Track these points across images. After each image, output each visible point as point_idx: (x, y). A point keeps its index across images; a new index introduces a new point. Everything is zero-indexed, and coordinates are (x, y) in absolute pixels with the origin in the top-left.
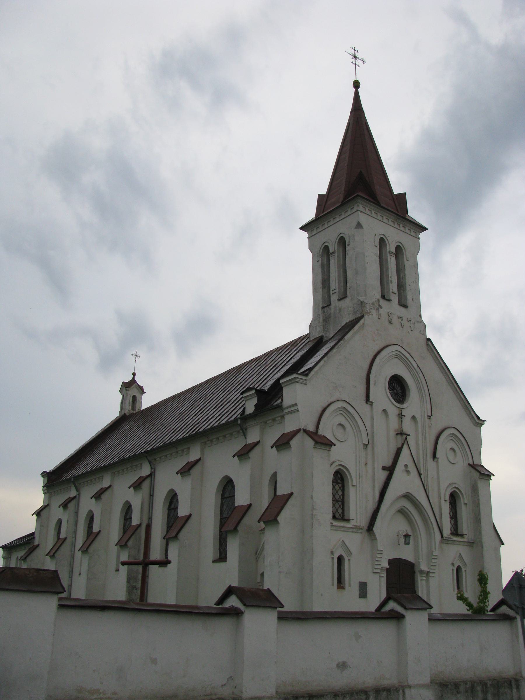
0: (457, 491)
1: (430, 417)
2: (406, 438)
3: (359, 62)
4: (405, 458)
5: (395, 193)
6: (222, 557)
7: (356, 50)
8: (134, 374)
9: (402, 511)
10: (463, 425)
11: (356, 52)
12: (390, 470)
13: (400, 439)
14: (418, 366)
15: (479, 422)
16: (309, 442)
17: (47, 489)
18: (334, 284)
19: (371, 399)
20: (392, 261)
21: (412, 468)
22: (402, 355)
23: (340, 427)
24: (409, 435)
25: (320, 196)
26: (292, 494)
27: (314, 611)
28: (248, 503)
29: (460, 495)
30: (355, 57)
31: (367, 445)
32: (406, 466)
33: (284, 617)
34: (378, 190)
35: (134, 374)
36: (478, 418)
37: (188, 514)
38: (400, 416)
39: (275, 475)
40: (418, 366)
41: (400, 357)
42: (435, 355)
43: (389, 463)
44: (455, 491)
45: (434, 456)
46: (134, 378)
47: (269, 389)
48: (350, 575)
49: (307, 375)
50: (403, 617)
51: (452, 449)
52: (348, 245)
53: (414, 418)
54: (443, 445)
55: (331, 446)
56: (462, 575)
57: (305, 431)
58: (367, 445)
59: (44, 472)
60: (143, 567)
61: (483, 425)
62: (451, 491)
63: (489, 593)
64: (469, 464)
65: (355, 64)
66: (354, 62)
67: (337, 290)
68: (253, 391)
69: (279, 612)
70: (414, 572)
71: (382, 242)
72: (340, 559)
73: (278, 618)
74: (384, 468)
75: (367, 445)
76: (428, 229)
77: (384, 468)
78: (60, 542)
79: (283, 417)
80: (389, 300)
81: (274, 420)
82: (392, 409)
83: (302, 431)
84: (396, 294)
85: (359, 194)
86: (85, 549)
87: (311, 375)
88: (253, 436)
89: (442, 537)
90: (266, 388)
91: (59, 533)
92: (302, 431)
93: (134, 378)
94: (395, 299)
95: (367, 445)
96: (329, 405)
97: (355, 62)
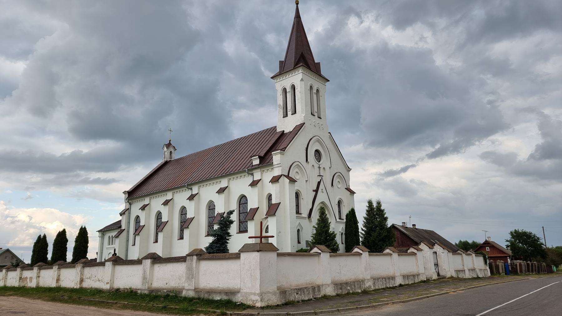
0: (298, 191)
5: (316, 62)
8: (170, 141)
12: (316, 191)
15: (349, 170)
16: (287, 181)
17: (511, 237)
20: (315, 96)
21: (324, 190)
23: (297, 173)
25: (281, 62)
32: (322, 189)
33: (280, 255)
34: (309, 62)
35: (170, 141)
36: (349, 168)
37: (224, 212)
38: (319, 167)
41: (318, 141)
43: (315, 188)
44: (340, 200)
45: (332, 185)
46: (170, 142)
48: (302, 237)
54: (336, 180)
55: (295, 182)
56: (300, 233)
57: (284, 175)
58: (307, 181)
63: (460, 241)
64: (345, 188)
67: (291, 110)
68: (258, 157)
71: (311, 87)
72: (298, 231)
73: (277, 255)
74: (314, 191)
77: (314, 191)
80: (314, 115)
81: (268, 170)
89: (336, 220)
93: (170, 142)
95: (307, 181)
96: (311, 139)
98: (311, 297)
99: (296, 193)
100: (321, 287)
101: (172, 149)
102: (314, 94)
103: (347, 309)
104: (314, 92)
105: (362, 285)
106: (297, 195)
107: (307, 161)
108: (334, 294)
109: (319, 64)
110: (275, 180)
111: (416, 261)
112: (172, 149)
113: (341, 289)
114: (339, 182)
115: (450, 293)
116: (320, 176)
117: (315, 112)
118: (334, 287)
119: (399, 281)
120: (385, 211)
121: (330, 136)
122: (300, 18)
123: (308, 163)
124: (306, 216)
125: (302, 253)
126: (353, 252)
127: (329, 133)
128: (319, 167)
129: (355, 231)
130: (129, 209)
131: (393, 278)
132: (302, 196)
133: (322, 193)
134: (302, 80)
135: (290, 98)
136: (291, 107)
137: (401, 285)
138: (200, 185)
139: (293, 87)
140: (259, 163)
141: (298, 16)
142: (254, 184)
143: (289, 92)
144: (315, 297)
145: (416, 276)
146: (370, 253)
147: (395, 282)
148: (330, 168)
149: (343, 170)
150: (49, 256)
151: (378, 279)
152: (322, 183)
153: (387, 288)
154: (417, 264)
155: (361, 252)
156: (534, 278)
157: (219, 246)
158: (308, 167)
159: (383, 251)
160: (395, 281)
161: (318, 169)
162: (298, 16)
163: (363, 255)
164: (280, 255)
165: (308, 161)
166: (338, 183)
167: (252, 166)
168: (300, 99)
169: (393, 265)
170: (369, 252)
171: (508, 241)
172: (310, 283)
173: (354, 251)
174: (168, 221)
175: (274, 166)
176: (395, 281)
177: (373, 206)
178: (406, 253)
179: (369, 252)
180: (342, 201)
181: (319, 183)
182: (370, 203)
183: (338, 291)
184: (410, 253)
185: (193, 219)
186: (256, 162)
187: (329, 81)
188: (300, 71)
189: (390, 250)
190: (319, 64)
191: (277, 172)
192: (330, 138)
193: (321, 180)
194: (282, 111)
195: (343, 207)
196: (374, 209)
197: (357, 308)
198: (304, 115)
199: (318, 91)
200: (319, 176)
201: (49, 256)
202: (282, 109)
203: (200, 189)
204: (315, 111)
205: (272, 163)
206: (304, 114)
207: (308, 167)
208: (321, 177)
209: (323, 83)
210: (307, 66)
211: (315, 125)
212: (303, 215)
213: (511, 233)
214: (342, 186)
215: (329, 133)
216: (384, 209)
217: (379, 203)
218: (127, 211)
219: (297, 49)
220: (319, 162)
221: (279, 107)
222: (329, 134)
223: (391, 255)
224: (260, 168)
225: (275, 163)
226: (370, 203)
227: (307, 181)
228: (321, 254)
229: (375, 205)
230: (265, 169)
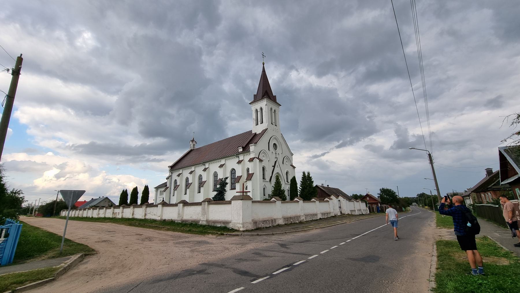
6: (199, 192)
7: (264, 55)
8: (193, 138)
10: (289, 155)
12: (274, 166)
14: (267, 256)
16: (258, 160)
20: (273, 114)
28: (241, 175)
30: (263, 55)
33: (253, 202)
34: (270, 95)
35: (193, 138)
40: (267, 256)
41: (275, 138)
43: (273, 165)
51: (287, 161)
53: (278, 154)
57: (256, 158)
59: (169, 166)
70: (204, 163)
74: (273, 166)
77: (273, 166)
80: (273, 124)
106: (264, 169)
108: (283, 224)
110: (251, 160)
113: (287, 221)
120: (312, 178)
125: (266, 201)
131: (316, 215)
134: (266, 105)
137: (320, 219)
139: (261, 109)
140: (242, 151)
141: (264, 71)
142: (239, 162)
150: (129, 201)
158: (269, 153)
161: (275, 154)
162: (264, 71)
164: (253, 202)
171: (378, 194)
179: (303, 200)
181: (276, 162)
182: (304, 173)
184: (325, 201)
186: (241, 150)
187: (281, 105)
188: (265, 100)
191: (252, 156)
201: (129, 201)
207: (269, 153)
212: (267, 180)
213: (380, 189)
214: (288, 164)
217: (309, 173)
219: (263, 88)
225: (251, 151)
226: (304, 173)
229: (306, 174)
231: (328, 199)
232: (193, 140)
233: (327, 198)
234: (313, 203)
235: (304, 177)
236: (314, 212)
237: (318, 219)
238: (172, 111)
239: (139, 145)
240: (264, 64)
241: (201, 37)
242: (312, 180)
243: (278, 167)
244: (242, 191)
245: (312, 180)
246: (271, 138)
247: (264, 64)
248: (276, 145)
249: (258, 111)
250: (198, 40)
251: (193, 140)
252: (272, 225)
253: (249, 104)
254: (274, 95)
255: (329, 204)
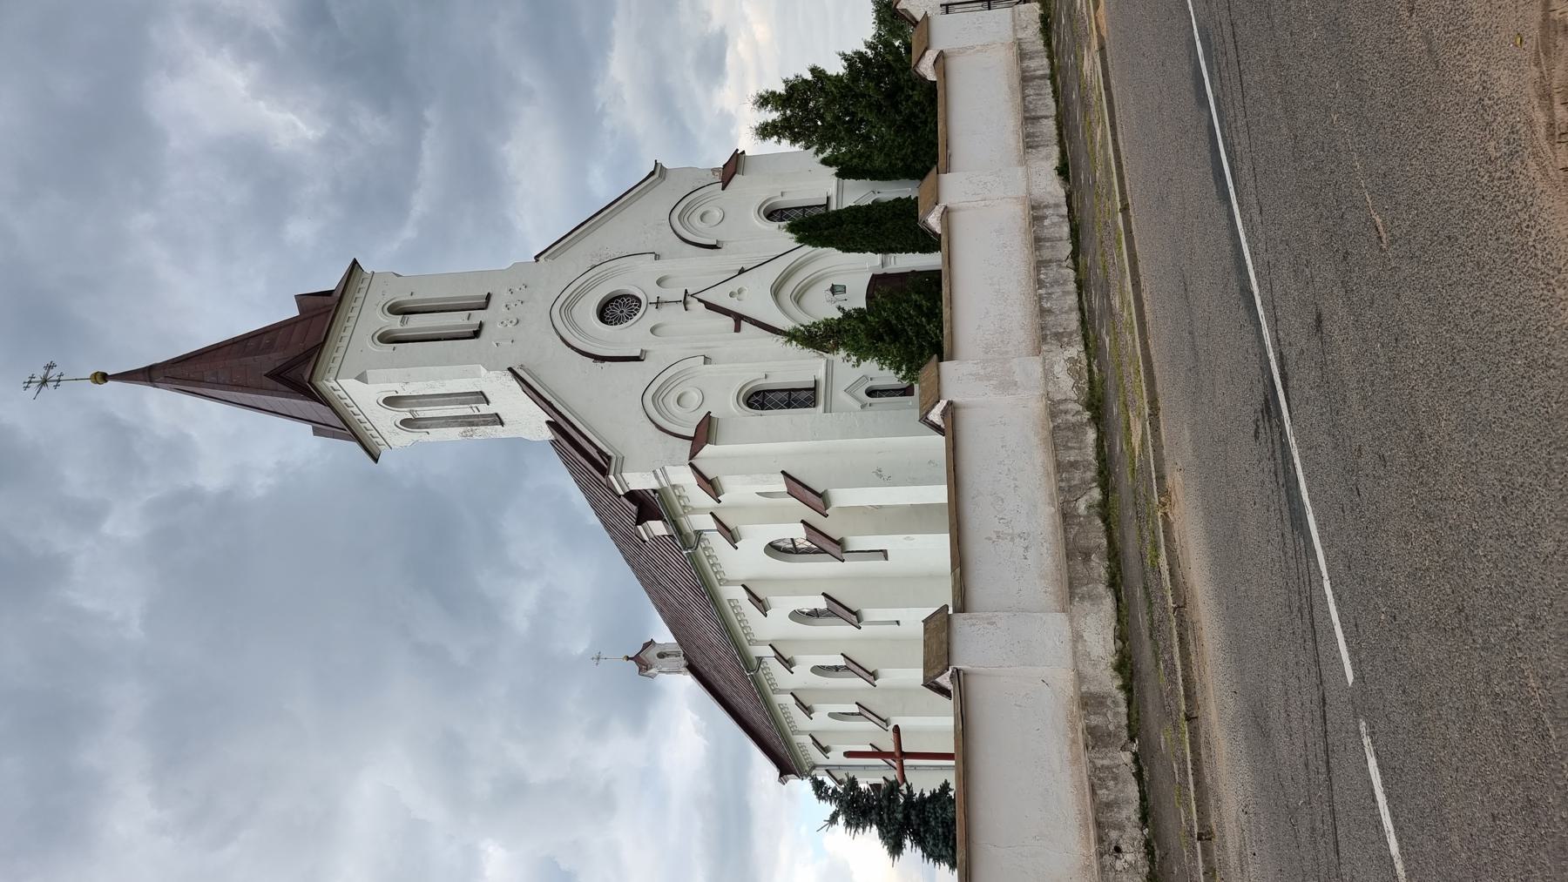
1: (656, 255)
2: (692, 296)
3: (53, 374)
4: (719, 297)
8: (628, 658)
9: (797, 299)
11: (33, 380)
12: (739, 318)
13: (693, 303)
16: (708, 450)
18: (465, 410)
19: (637, 353)
20: (417, 323)
21: (733, 285)
22: (565, 306)
24: (686, 291)
26: (783, 472)
27: (946, 501)
29: (769, 203)
30: (44, 382)
31: (705, 357)
32: (731, 295)
33: (962, 602)
35: (628, 658)
36: (652, 174)
39: (758, 493)
41: (568, 308)
42: (560, 248)
43: (730, 321)
46: (632, 659)
47: (635, 505)
49: (609, 458)
50: (950, 403)
52: (397, 392)
53: (659, 282)
60: (905, 758)
61: (664, 165)
62: (763, 216)
64: (723, 189)
65: (59, 381)
66: (55, 383)
69: (955, 611)
71: (388, 338)
72: (871, 393)
74: (737, 329)
75: (705, 357)
76: (355, 259)
77: (737, 329)
78: (852, 666)
79: (674, 487)
80: (481, 325)
82: (648, 317)
83: (692, 461)
84: (470, 314)
85: (307, 377)
86: (854, 617)
87: (610, 453)
88: (704, 522)
90: (634, 508)
91: (837, 668)
92: (692, 461)
93: (632, 659)
94: (478, 317)
97: (54, 381)
98: (1126, 757)
99: (750, 406)
100: (1084, 689)
101: (652, 654)
102: (405, 327)
103: (1196, 785)
104: (400, 327)
105: (1069, 417)
106: (758, 399)
107: (638, 357)
108: (1108, 604)
109: (301, 299)
111: (969, 52)
112: (652, 654)
113: (1087, 557)
114: (702, 217)
115: (1104, 34)
116: (685, 303)
117: (470, 322)
118: (1082, 598)
119: (1051, 189)
120: (792, 77)
121: (547, 257)
122: (151, 366)
123: (646, 352)
124: (823, 362)
125: (950, 428)
126: (943, 426)
127: (537, 261)
128: (658, 304)
129: (867, 224)
130: (827, 770)
131: (1036, 214)
132: (759, 379)
133: (745, 294)
134: (362, 378)
135: (431, 408)
136: (461, 406)
137: (1063, 171)
138: (746, 642)
139: (392, 401)
140: (660, 522)
141: (149, 375)
143: (410, 412)
144: (1125, 734)
145: (1026, 63)
146: (945, 359)
147: (1052, 202)
148: (657, 257)
149: (659, 203)
151: (1043, 312)
152: (710, 296)
153: (1075, 255)
154: (978, 51)
155: (943, 403)
156: (1139, 451)
157: (934, 839)
158: (662, 352)
159: (935, 233)
160: (1046, 207)
161: (665, 309)
162: (149, 375)
163: (955, 399)
164: (962, 602)
165: (638, 354)
166: (706, 218)
167: (669, 536)
168: (429, 383)
169: (987, 203)
170: (942, 361)
172: (1070, 736)
173: (938, 424)
174: (857, 703)
175: (665, 485)
176: (1046, 207)
177: (774, 121)
178: (943, 237)
179: (941, 359)
180: (764, 203)
181: (710, 306)
183: (1096, 575)
184: (937, 74)
185: (847, 658)
186: (657, 528)
187: (355, 262)
188: (334, 384)
189: (929, 212)
190: (301, 299)
191: (683, 477)
192: (553, 257)
193: (700, 300)
194: (482, 428)
195: (786, 198)
196: (786, 119)
197: (1189, 718)
198: (483, 371)
199: (398, 310)
200: (688, 306)
202: (474, 428)
203: (758, 639)
204: (466, 322)
205: (655, 491)
206: (479, 369)
207: (662, 352)
208: (689, 298)
209: (365, 285)
210: (312, 356)
211: (515, 321)
212: (821, 375)
214: (718, 201)
215: (537, 261)
216: (785, 82)
217: (765, 101)
218: (834, 773)
219: (258, 389)
220: (639, 300)
221: (471, 436)
222: (541, 258)
223: (947, 211)
224: (676, 516)
225: (654, 485)
227: (707, 360)
228: (958, 667)
229: (772, 115)
230: (678, 505)
231: (923, 54)
232: (637, 659)
233: (916, 65)
234: (956, 67)
235: (791, 129)
236: (1013, 215)
237: (1062, 193)
238: (524, 601)
239: (697, 718)
240: (104, 377)
241: (87, 516)
242: (809, 76)
243: (740, 291)
244: (905, 749)
245: (809, 76)
246: (569, 345)
247: (104, 377)
248: (612, 300)
249: (409, 416)
250: (108, 527)
251: (637, 659)
252: (1123, 749)
253: (376, 460)
254: (296, 313)
255: (962, 51)
